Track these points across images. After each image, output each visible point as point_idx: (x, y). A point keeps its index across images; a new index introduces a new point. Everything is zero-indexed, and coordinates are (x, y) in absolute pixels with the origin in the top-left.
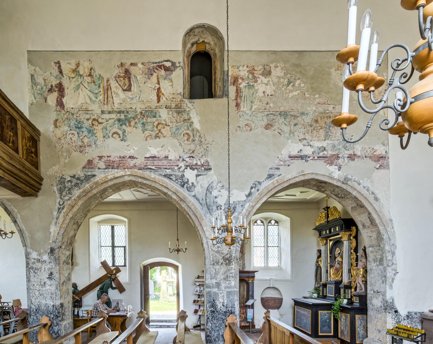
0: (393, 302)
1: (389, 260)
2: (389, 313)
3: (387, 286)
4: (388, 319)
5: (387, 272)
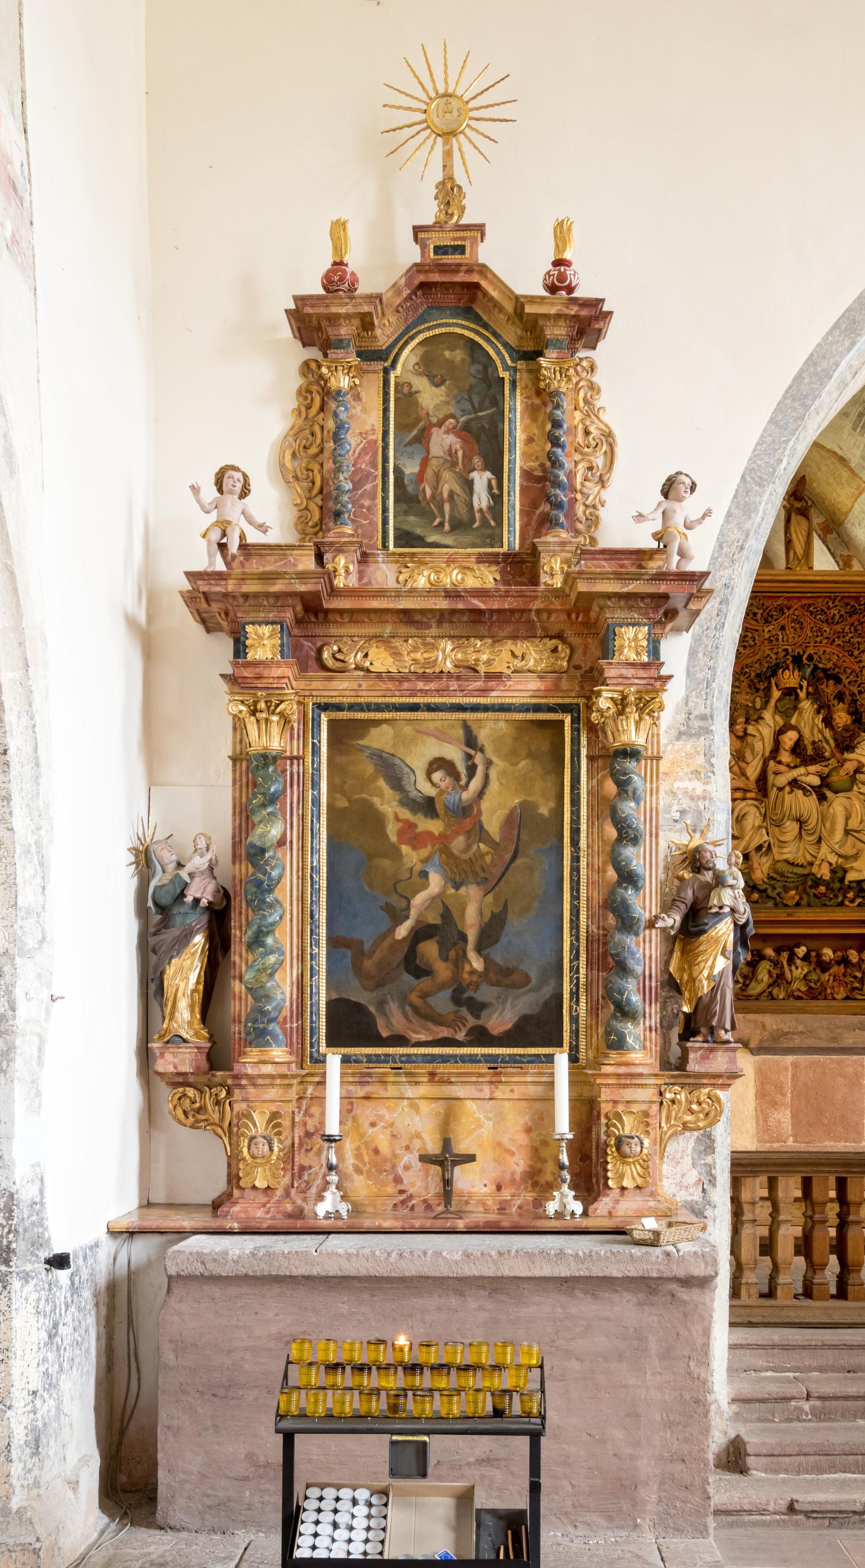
0: (37, 1206)
1: (29, 912)
2: (26, 1277)
3: (17, 1086)
4: (18, 1322)
5: (19, 993)
